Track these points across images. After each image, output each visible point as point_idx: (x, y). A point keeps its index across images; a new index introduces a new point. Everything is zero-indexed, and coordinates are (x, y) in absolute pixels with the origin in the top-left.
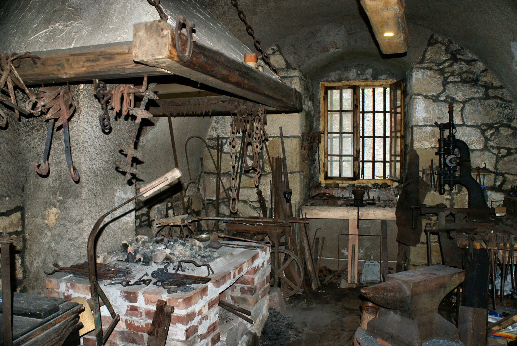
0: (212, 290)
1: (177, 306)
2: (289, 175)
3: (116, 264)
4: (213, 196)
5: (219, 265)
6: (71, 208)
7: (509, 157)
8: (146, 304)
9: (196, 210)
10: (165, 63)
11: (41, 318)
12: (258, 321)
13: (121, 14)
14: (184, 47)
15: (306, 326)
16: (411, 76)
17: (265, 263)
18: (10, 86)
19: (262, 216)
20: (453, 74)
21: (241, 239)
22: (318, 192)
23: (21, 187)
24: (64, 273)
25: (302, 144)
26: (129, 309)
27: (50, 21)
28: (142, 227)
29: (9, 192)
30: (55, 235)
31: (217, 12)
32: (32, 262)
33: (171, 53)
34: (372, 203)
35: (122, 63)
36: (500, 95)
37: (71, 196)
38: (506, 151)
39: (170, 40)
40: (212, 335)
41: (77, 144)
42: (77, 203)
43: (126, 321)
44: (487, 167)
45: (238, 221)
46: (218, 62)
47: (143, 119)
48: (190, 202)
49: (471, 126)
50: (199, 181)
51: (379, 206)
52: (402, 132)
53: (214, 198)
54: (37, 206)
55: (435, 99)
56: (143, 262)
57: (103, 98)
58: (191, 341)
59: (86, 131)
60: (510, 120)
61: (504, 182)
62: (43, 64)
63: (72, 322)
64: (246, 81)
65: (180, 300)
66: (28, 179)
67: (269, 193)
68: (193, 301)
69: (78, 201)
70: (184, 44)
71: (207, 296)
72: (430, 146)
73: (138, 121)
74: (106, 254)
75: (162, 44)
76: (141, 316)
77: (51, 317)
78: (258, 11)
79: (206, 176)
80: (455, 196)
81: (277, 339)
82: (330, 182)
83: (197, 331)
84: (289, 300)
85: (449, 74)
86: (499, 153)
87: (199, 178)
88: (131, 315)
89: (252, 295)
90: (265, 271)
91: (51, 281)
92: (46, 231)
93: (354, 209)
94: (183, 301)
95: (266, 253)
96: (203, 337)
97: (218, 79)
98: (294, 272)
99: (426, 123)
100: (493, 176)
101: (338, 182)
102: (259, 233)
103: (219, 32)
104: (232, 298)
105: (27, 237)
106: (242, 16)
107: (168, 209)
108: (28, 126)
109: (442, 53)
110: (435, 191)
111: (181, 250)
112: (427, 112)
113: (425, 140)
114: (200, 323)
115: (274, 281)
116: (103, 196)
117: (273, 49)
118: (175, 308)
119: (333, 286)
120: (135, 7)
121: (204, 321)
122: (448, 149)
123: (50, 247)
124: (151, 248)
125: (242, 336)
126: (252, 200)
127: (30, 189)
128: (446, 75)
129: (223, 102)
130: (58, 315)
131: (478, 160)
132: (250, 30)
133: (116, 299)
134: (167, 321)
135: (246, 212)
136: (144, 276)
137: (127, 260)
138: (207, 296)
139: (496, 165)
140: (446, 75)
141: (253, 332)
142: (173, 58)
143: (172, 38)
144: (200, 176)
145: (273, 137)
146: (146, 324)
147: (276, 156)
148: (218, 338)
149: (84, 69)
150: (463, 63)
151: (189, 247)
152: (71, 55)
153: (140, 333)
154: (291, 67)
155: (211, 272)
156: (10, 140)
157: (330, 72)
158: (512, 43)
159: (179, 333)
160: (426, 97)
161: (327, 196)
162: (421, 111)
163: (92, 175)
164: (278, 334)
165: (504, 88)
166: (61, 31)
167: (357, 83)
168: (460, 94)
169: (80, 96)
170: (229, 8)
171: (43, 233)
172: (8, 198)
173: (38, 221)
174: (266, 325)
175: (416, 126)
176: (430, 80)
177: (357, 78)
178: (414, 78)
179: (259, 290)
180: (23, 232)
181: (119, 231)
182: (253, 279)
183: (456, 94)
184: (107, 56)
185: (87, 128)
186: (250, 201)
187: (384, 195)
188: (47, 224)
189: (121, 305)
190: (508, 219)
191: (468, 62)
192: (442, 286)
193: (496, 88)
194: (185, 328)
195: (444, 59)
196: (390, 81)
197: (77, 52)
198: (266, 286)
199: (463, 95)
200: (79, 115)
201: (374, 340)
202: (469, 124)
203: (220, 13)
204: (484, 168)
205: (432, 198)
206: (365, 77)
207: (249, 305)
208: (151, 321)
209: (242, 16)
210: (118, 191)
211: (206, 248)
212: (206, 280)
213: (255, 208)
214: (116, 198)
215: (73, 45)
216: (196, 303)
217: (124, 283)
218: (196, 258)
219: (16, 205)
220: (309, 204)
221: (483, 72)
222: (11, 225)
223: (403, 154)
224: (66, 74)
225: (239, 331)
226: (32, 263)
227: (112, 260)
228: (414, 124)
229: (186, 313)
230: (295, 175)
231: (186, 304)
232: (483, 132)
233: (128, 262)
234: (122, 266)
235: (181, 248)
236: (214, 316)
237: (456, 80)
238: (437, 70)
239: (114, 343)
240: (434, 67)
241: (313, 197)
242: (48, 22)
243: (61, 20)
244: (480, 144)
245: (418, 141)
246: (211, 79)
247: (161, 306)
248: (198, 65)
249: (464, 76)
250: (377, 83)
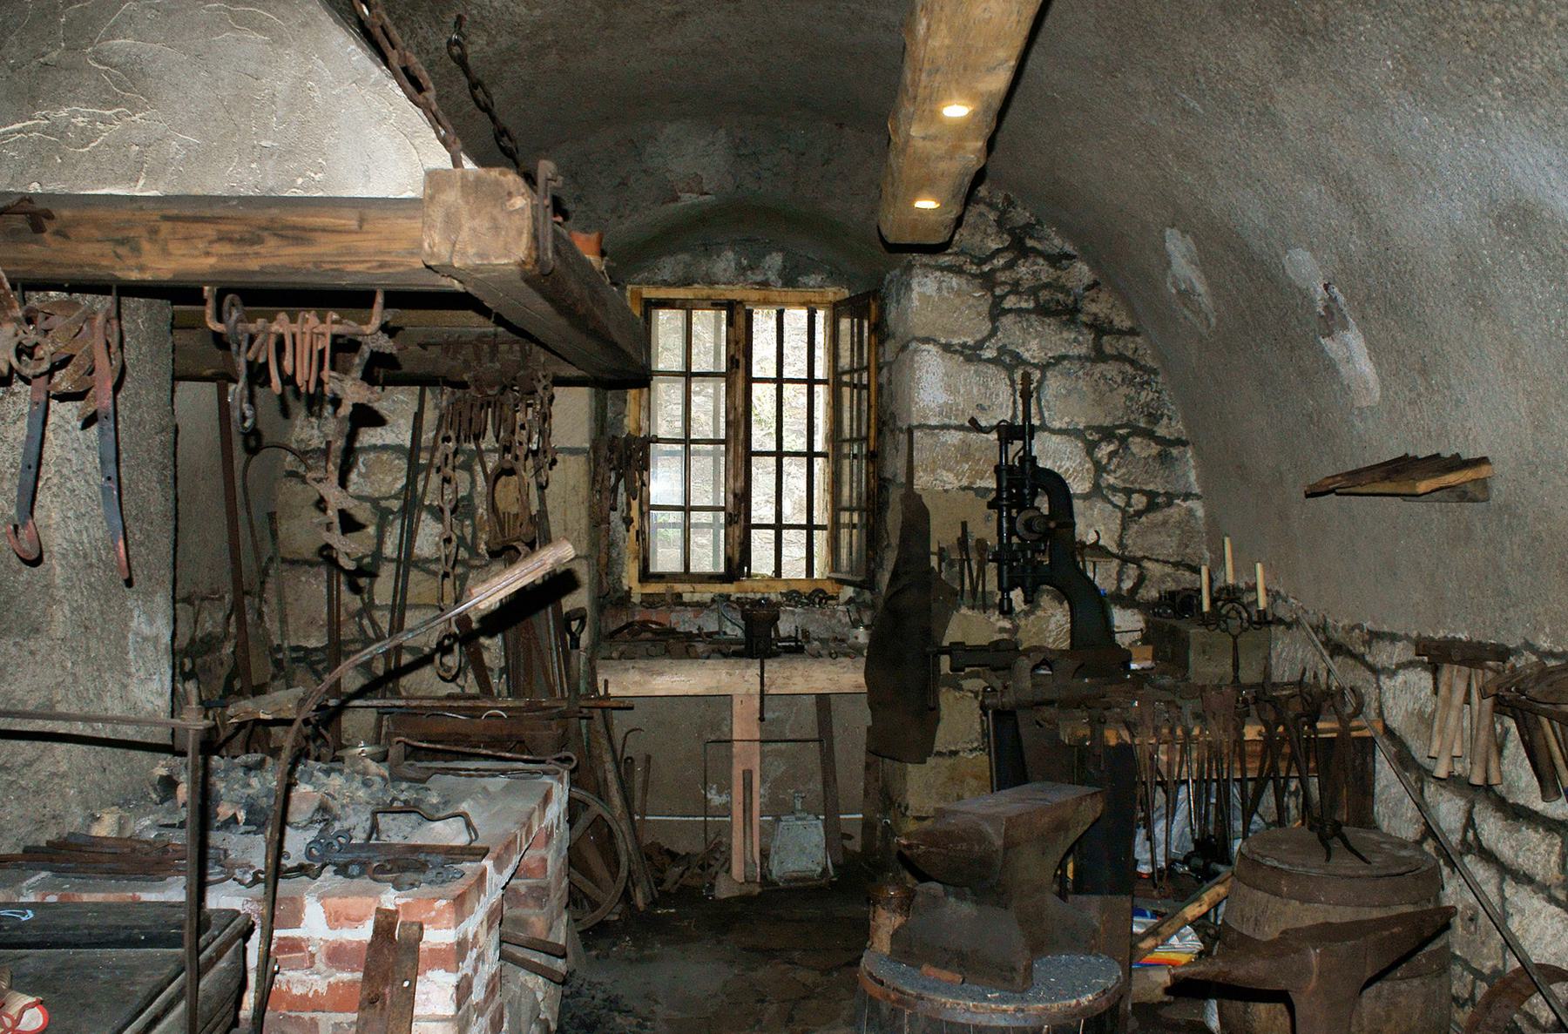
1: (432, 922)
7: (1151, 516)
13: (292, 111)
15: (656, 1002)
16: (908, 287)
20: (1015, 288)
22: (624, 619)
34: (796, 648)
35: (340, 255)
36: (1129, 353)
38: (1144, 499)
42: (32, 653)
44: (1102, 542)
47: (355, 406)
49: (1060, 432)
50: (263, 590)
51: (817, 656)
52: (872, 443)
55: (971, 354)
56: (247, 822)
60: (1154, 418)
61: (1141, 581)
69: (41, 644)
72: (957, 484)
73: (345, 410)
80: (1023, 623)
82: (654, 588)
85: (1007, 289)
86: (1128, 504)
93: (748, 667)
99: (947, 421)
100: (1115, 563)
101: (679, 587)
109: (989, 230)
110: (973, 608)
112: (950, 389)
113: (944, 467)
116: (103, 630)
119: (688, 896)
120: (338, 97)
122: (1020, 492)
128: (998, 291)
131: (1094, 524)
132: (505, 138)
134: (410, 964)
139: (1121, 537)
140: (998, 291)
146: (329, 985)
149: (212, 261)
150: (1041, 261)
152: (167, 218)
153: (306, 1015)
157: (659, 256)
158: (1168, 231)
160: (947, 348)
161: (652, 631)
162: (933, 387)
165: (1138, 335)
166: (86, 137)
167: (735, 293)
168: (1034, 344)
175: (921, 427)
176: (957, 301)
177: (736, 277)
178: (914, 295)
182: (544, 860)
183: (1023, 344)
184: (290, 233)
185: (69, 416)
187: (817, 623)
190: (1163, 673)
191: (1056, 260)
192: (1061, 826)
193: (1121, 333)
194: (453, 979)
195: (994, 246)
196: (834, 293)
199: (1042, 348)
201: (916, 973)
202: (1057, 425)
204: (1095, 546)
205: (970, 626)
206: (759, 278)
210: (136, 613)
214: (130, 636)
220: (614, 655)
221: (1089, 288)
223: (873, 505)
224: (142, 268)
228: (915, 423)
232: (1091, 448)
237: (1024, 305)
238: (974, 276)
240: (967, 267)
241: (612, 635)
244: (1083, 479)
245: (925, 471)
247: (385, 926)
249: (1044, 295)
250: (792, 294)
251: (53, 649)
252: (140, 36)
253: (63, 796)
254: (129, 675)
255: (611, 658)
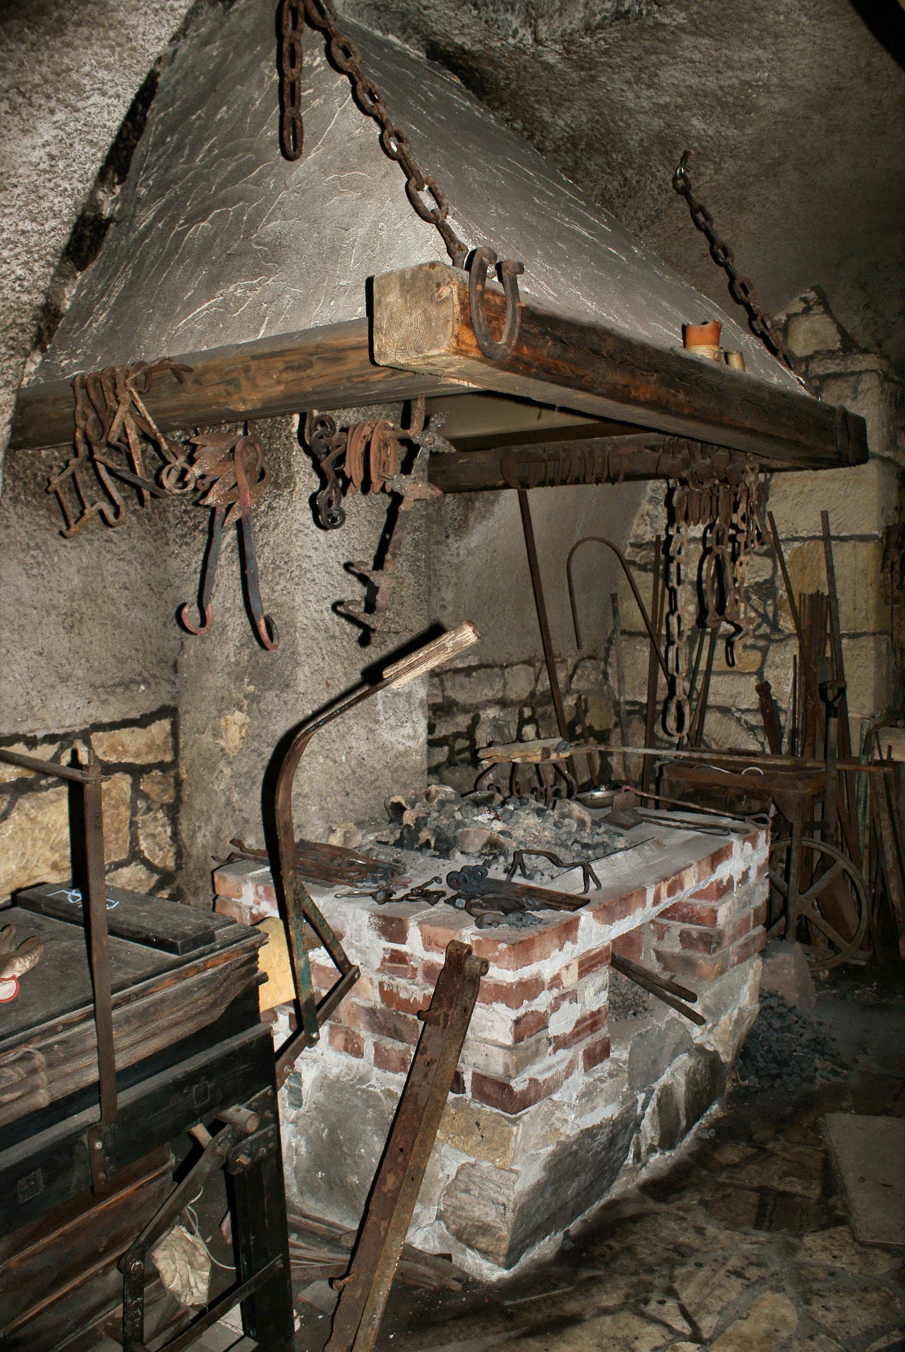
0: (591, 929)
1: (496, 960)
2: (845, 641)
3: (371, 849)
4: (641, 694)
5: (613, 870)
6: (274, 714)
8: (427, 950)
9: (597, 728)
10: (450, 364)
11: (176, 953)
12: (726, 1020)
14: (494, 323)
17: (753, 874)
18: (133, 437)
19: (768, 750)
21: (693, 806)
23: (170, 663)
24: (252, 864)
25: (885, 558)
26: (387, 956)
27: (219, 282)
28: (456, 764)
29: (146, 674)
30: (241, 775)
31: (640, 213)
32: (194, 832)
33: (459, 341)
37: (273, 684)
39: (458, 308)
40: (588, 1041)
41: (286, 563)
43: (381, 984)
45: (701, 760)
46: (596, 352)
48: (581, 710)
50: (607, 655)
53: (644, 700)
54: (203, 705)
57: (328, 453)
58: (527, 1048)
59: (306, 531)
62: (197, 382)
63: (243, 970)
64: (681, 396)
65: (503, 946)
66: (186, 643)
67: (788, 689)
68: (537, 951)
69: (289, 696)
70: (496, 315)
71: (575, 942)
74: (351, 825)
75: (438, 319)
76: (413, 977)
77: (196, 952)
78: (750, 199)
79: (623, 642)
81: (779, 1076)
83: (546, 1027)
84: (830, 977)
87: (606, 645)
88: (393, 972)
89: (709, 953)
90: (750, 893)
91: (225, 880)
92: (222, 765)
94: (509, 949)
95: (754, 846)
96: (561, 1043)
97: (599, 394)
98: (846, 903)
102: (752, 795)
103: (634, 268)
104: (660, 956)
105: (185, 777)
106: (700, 217)
107: (523, 722)
108: (185, 523)
111: (529, 826)
114: (555, 1007)
115: (780, 920)
117: (805, 300)
118: (491, 964)
120: (398, 230)
121: (565, 1004)
123: (228, 803)
124: (458, 816)
125: (675, 1055)
126: (744, 707)
127: (189, 666)
129: (653, 448)
130: (213, 950)
133: (359, 931)
134: (470, 994)
135: (727, 738)
136: (430, 883)
137: (399, 844)
138: (575, 942)
141: (709, 1048)
142: (466, 351)
143: (462, 303)
144: (610, 641)
145: (804, 539)
147: (811, 591)
148: (605, 1052)
149: (282, 388)
151: (551, 820)
154: (856, 346)
155: (593, 886)
156: (149, 555)
159: (498, 1025)
163: (320, 636)
164: (782, 1064)
166: (239, 301)
169: (292, 447)
170: (671, 200)
171: (215, 770)
172: (143, 687)
173: (205, 741)
174: (751, 1035)
179: (731, 943)
180: (175, 764)
181: (386, 772)
182: (714, 912)
186: (738, 710)
188: (222, 750)
189: (364, 944)
194: (514, 1014)
197: (267, 350)
198: (753, 933)
200: (291, 493)
203: (648, 217)
207: (701, 977)
208: (432, 990)
209: (700, 217)
211: (596, 824)
212: (576, 903)
213: (751, 729)
215: (262, 332)
216: (545, 956)
217: (381, 896)
218: (566, 847)
219: (160, 703)
222: (150, 747)
225: (668, 1041)
226: (193, 837)
227: (365, 841)
229: (517, 979)
230: (863, 641)
231: (517, 957)
233: (402, 846)
234: (384, 856)
235: (533, 820)
236: (594, 994)
239: (354, 1033)
242: (213, 283)
243: (241, 276)
246: (582, 396)
248: (536, 364)
251: (297, 700)
252: (285, 217)
253: (306, 811)
254: (377, 722)
255: (896, 726)
